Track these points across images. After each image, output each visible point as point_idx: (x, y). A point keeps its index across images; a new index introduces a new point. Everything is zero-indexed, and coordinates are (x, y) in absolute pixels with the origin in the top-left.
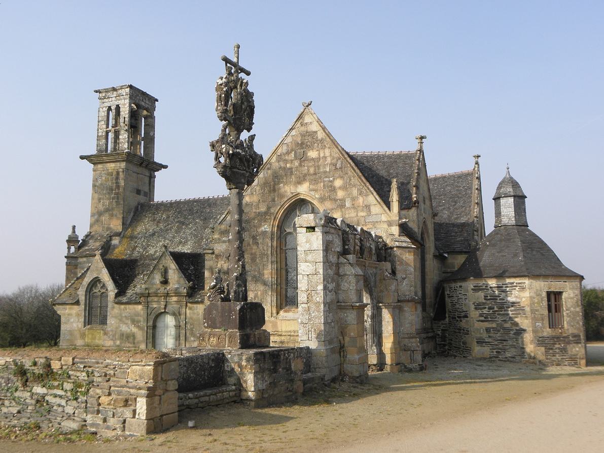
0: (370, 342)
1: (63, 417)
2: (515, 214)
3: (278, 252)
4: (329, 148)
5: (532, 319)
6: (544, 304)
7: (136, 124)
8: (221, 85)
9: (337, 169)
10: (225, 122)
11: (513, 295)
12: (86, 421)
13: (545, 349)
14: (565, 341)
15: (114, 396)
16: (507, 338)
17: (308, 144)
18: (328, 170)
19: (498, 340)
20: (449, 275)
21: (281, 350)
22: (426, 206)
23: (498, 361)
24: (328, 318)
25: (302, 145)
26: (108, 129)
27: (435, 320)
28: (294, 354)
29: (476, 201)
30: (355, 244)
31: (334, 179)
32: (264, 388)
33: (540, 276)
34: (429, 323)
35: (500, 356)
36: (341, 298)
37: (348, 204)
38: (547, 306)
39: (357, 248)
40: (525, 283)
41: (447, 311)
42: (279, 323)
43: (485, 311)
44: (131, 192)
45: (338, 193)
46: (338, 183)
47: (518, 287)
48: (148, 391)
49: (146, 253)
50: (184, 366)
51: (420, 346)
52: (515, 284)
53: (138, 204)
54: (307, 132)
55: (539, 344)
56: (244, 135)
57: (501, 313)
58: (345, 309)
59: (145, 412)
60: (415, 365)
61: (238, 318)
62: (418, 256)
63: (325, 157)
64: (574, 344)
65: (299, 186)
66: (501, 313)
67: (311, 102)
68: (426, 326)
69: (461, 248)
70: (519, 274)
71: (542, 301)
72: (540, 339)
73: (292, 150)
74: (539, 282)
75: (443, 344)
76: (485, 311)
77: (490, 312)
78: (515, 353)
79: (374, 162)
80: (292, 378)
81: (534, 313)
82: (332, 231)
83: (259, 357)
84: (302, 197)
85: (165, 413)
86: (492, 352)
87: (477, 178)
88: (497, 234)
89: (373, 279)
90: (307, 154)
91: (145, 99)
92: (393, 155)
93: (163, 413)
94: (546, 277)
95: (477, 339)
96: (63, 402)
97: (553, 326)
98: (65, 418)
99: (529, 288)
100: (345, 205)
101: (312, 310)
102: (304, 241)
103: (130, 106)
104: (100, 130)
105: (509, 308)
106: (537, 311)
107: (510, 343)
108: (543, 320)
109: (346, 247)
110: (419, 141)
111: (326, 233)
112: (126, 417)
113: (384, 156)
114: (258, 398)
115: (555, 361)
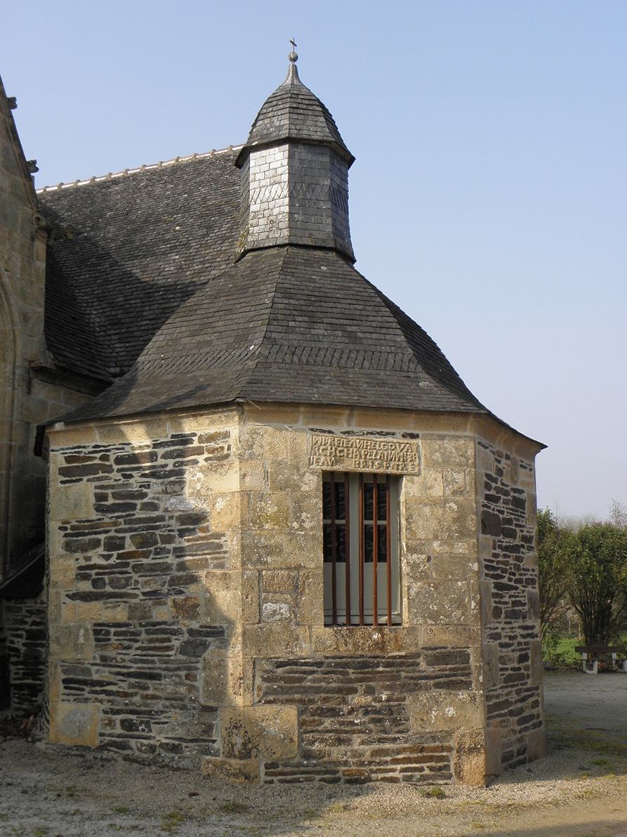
2: (291, 205)
5: (247, 585)
13: (301, 713)
14: (395, 678)
19: (129, 675)
27: (9, 599)
35: (133, 742)
38: (320, 534)
40: (226, 435)
47: (206, 455)
52: (196, 444)
55: (275, 692)
57: (145, 561)
64: (435, 692)
66: (145, 561)
71: (299, 509)
72: (280, 670)
74: (289, 435)
75: (29, 686)
77: (112, 561)
78: (180, 732)
81: (259, 561)
86: (111, 723)
94: (322, 409)
95: (64, 672)
97: (362, 615)
99: (241, 457)
105: (169, 539)
107: (168, 685)
108: (297, 589)
115: (346, 763)
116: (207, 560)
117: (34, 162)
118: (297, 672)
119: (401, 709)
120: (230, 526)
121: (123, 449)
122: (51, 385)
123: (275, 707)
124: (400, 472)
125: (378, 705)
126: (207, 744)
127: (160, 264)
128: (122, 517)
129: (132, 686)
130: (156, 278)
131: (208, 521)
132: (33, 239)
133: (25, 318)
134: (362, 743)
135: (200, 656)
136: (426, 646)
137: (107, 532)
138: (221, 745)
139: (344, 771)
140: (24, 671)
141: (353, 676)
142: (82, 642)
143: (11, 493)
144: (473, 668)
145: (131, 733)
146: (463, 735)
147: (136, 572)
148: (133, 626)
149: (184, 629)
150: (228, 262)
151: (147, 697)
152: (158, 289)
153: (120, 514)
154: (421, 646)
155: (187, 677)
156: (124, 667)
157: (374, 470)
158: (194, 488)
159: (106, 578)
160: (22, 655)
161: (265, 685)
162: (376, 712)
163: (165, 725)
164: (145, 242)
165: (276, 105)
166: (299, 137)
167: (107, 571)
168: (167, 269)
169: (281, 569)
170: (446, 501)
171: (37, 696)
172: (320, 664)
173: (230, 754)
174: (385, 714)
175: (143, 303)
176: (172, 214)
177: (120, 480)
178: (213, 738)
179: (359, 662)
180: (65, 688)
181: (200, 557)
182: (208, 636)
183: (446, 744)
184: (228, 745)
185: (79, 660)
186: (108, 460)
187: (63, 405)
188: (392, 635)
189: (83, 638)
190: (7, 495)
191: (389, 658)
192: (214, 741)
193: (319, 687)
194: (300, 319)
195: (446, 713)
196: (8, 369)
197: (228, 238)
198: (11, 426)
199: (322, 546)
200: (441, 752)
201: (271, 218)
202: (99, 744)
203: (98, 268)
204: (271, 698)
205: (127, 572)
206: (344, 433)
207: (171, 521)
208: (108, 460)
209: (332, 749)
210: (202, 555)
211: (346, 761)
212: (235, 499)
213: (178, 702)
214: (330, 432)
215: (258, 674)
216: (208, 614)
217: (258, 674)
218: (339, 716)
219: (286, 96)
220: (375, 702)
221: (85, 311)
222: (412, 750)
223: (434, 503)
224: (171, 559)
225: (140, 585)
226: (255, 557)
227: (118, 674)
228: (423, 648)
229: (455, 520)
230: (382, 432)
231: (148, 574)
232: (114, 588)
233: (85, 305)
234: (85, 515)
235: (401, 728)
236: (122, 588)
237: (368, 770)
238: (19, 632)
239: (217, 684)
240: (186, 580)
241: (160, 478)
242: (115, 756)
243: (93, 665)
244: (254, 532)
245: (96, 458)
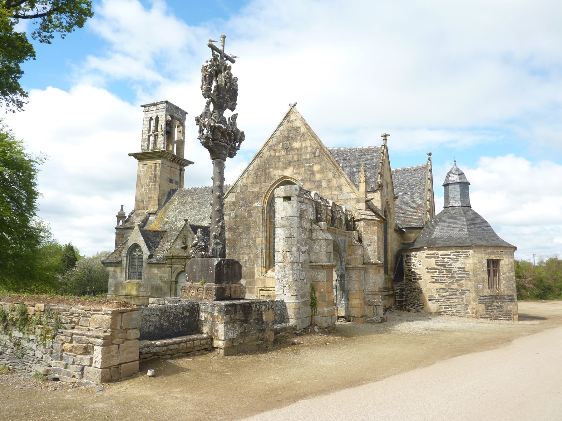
0: (339, 297)
1: (33, 361)
3: (268, 225)
4: (310, 140)
5: (475, 281)
6: (485, 270)
7: (171, 130)
8: (206, 67)
9: (316, 156)
10: (209, 99)
11: (459, 262)
12: (51, 366)
13: (485, 306)
15: (75, 344)
17: (293, 136)
18: (308, 157)
19: (446, 298)
20: (406, 245)
21: (254, 303)
22: (388, 190)
24: (301, 276)
25: (288, 138)
26: (149, 134)
27: (395, 281)
28: (266, 306)
29: (429, 188)
30: (327, 214)
31: (313, 165)
32: (235, 337)
33: (482, 246)
34: (390, 284)
35: (448, 311)
36: (313, 259)
37: (324, 184)
38: (487, 271)
39: (329, 217)
40: (469, 252)
41: (405, 274)
42: (267, 280)
43: (436, 274)
44: (165, 181)
45: (316, 176)
46: (316, 168)
48: (104, 339)
49: (174, 226)
50: (157, 315)
51: (382, 302)
52: (461, 253)
53: (171, 190)
54: (292, 128)
55: (480, 302)
56: (227, 114)
58: (316, 268)
59: (101, 360)
60: (378, 318)
61: (215, 272)
62: (381, 229)
63: (306, 147)
64: (509, 303)
65: (285, 170)
66: (449, 276)
67: (296, 103)
68: (388, 286)
69: (416, 225)
70: (464, 245)
71: (483, 267)
73: (280, 142)
76: (436, 274)
77: (440, 275)
78: (460, 309)
79: (347, 155)
80: (264, 328)
82: (307, 201)
83: (229, 308)
84: (287, 179)
85: (124, 362)
87: (430, 170)
88: (446, 213)
89: (342, 245)
90: (292, 144)
91: (178, 112)
92: (363, 149)
93: (121, 362)
95: (428, 297)
96: (34, 346)
97: (491, 287)
98: (35, 362)
100: (322, 186)
101: (287, 268)
102: (281, 209)
103: (166, 117)
104: (144, 134)
105: (455, 272)
107: (456, 300)
108: (483, 282)
109: (319, 216)
110: (383, 138)
111: (300, 202)
112: (84, 364)
113: (356, 150)
114: (228, 346)
115: (493, 316)
119: (502, 306)
123: (481, 305)
129: (446, 300)
155: (461, 299)
159: (439, 279)
172: (488, 297)
173: (473, 313)
176: (400, 184)
197: (419, 192)
216: (466, 286)
223: (507, 265)
224: (456, 276)
225: (448, 281)
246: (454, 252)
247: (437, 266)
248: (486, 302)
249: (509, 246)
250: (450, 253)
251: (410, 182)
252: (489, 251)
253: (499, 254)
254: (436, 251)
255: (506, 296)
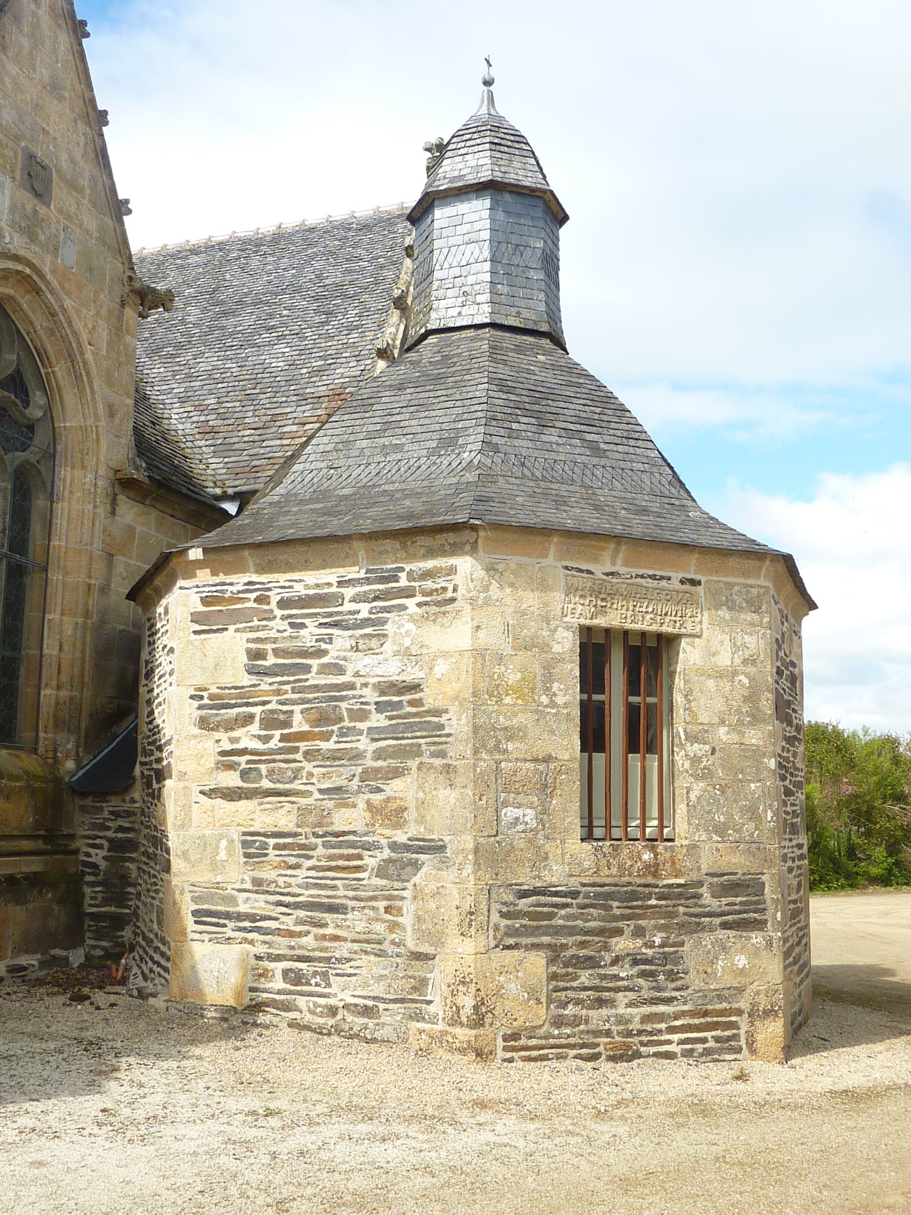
5: (482, 782)
13: (551, 961)
16: (341, 894)
19: (297, 906)
23: (286, 1033)
27: (84, 795)
35: (301, 1001)
38: (577, 712)
40: (452, 571)
43: (247, 738)
47: (419, 599)
52: (403, 582)
55: (515, 932)
57: (324, 745)
64: (722, 934)
66: (324, 745)
71: (549, 678)
72: (523, 904)
76: (247, 738)
78: (378, 990)
95: (195, 900)
97: (608, 826)
105: (361, 715)
106: (510, 739)
108: (545, 788)
115: (608, 1033)
116: (420, 745)
117: (127, 201)
118: (545, 905)
119: (677, 959)
120: (456, 698)
121: (292, 587)
122: (140, 505)
124: (676, 631)
125: (650, 952)
126: (418, 1005)
127: (264, 357)
128: (288, 683)
129: (300, 922)
130: (259, 376)
131: (422, 690)
132: (123, 305)
133: (111, 412)
134: (630, 1005)
135: (408, 881)
136: (710, 871)
137: (264, 703)
138: (441, 1008)
139: (607, 1044)
140: (104, 895)
141: (617, 912)
142: (225, 858)
143: (88, 650)
144: (769, 902)
145: (299, 988)
146: (757, 993)
147: (309, 761)
148: (303, 837)
149: (384, 842)
150: (359, 358)
151: (324, 937)
152: (264, 390)
153: (285, 678)
154: (704, 872)
155: (387, 910)
156: (288, 894)
157: (645, 627)
158: (400, 644)
159: (263, 768)
160: (102, 873)
161: (504, 922)
162: (647, 962)
163: (352, 978)
164: (241, 328)
165: (470, 139)
166: (506, 181)
167: (264, 758)
168: (273, 365)
169: (526, 760)
170: (735, 673)
171: (123, 930)
172: (574, 894)
173: (455, 1021)
174: (659, 965)
175: (243, 406)
176: (277, 294)
177: (285, 630)
178: (428, 998)
179: (626, 892)
180: (196, 922)
181: (410, 741)
182: (421, 853)
183: (735, 1006)
184: (451, 1008)
185: (218, 883)
186: (269, 603)
187: (155, 534)
188: (668, 855)
189: (225, 852)
190: (83, 652)
191: (664, 886)
192: (429, 1002)
193: (575, 927)
194: (525, 420)
195: (736, 962)
196: (88, 480)
197: (357, 327)
198: (91, 558)
199: (579, 729)
200: (730, 1016)
201: (464, 289)
202: (249, 1003)
203: (178, 360)
204: (511, 941)
205: (295, 761)
206: (607, 574)
207: (364, 689)
208: (269, 603)
209: (592, 1013)
210: (412, 738)
211: (609, 1029)
212: (465, 661)
213: (373, 946)
214: (589, 572)
215: (495, 907)
216: (421, 820)
217: (495, 907)
218: (600, 967)
219: (484, 128)
220: (646, 948)
221: (163, 414)
222: (692, 1014)
223: (720, 675)
224: (364, 744)
226: (491, 743)
227: (280, 904)
228: (706, 874)
229: (746, 699)
230: (655, 575)
231: (328, 763)
232: (274, 783)
233: (162, 406)
234: (232, 680)
235: (679, 983)
236: (287, 783)
237: (636, 1042)
238: (98, 841)
239: (435, 921)
240: (387, 772)
241: (349, 629)
242: (275, 1020)
243: (240, 891)
244: (491, 708)
245: (248, 599)
246: (362, 574)
247: (254, 680)
248: (558, 931)
249: (744, 546)
250: (340, 584)
251: (327, 282)
252: (598, 570)
253: (669, 597)
254: (255, 578)
255: (704, 890)
